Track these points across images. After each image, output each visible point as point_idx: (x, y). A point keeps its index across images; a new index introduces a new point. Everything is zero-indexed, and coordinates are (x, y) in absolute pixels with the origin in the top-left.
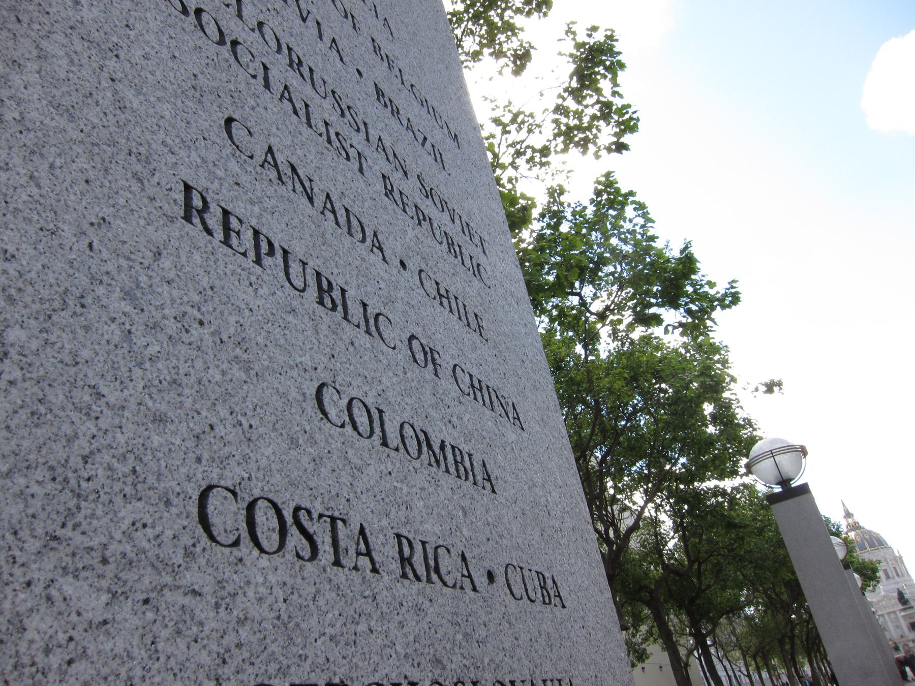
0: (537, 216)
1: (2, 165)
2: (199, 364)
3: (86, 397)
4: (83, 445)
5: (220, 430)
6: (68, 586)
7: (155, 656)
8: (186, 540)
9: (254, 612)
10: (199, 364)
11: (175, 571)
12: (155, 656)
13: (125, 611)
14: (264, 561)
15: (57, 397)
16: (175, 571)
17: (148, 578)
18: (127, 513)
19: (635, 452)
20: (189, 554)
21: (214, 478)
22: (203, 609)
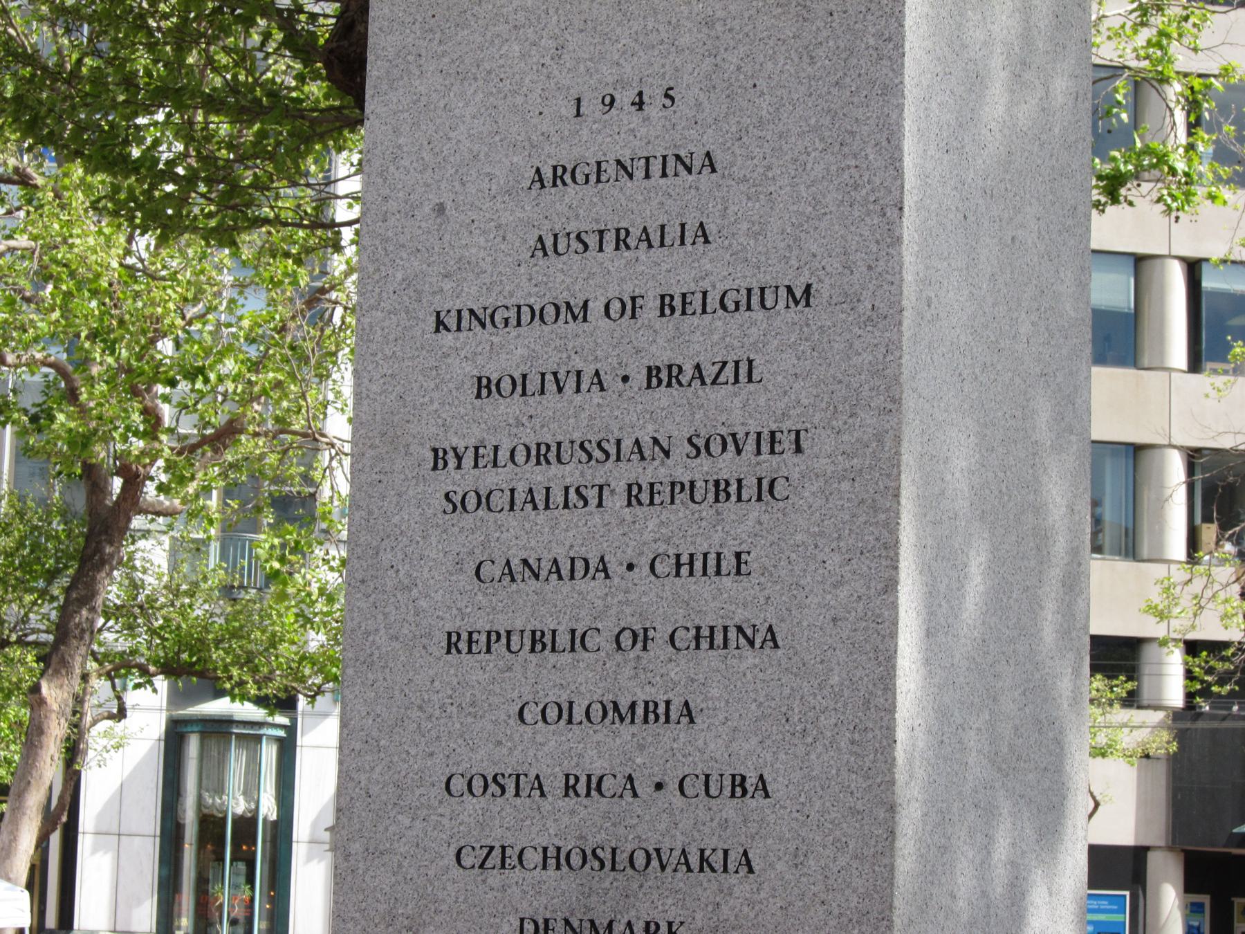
0: (1164, 624)
1: (492, 931)
2: (450, 724)
3: (404, 756)
4: (403, 773)
5: (458, 750)
6: (400, 817)
7: (426, 835)
8: (439, 798)
9: (466, 820)
10: (450, 724)
11: (435, 809)
12: (426, 835)
13: (418, 824)
14: (475, 800)
15: (396, 759)
16: (435, 809)
17: (425, 812)
18: (418, 792)
19: (47, 505)
20: (441, 802)
21: (454, 771)
22: (445, 821)
